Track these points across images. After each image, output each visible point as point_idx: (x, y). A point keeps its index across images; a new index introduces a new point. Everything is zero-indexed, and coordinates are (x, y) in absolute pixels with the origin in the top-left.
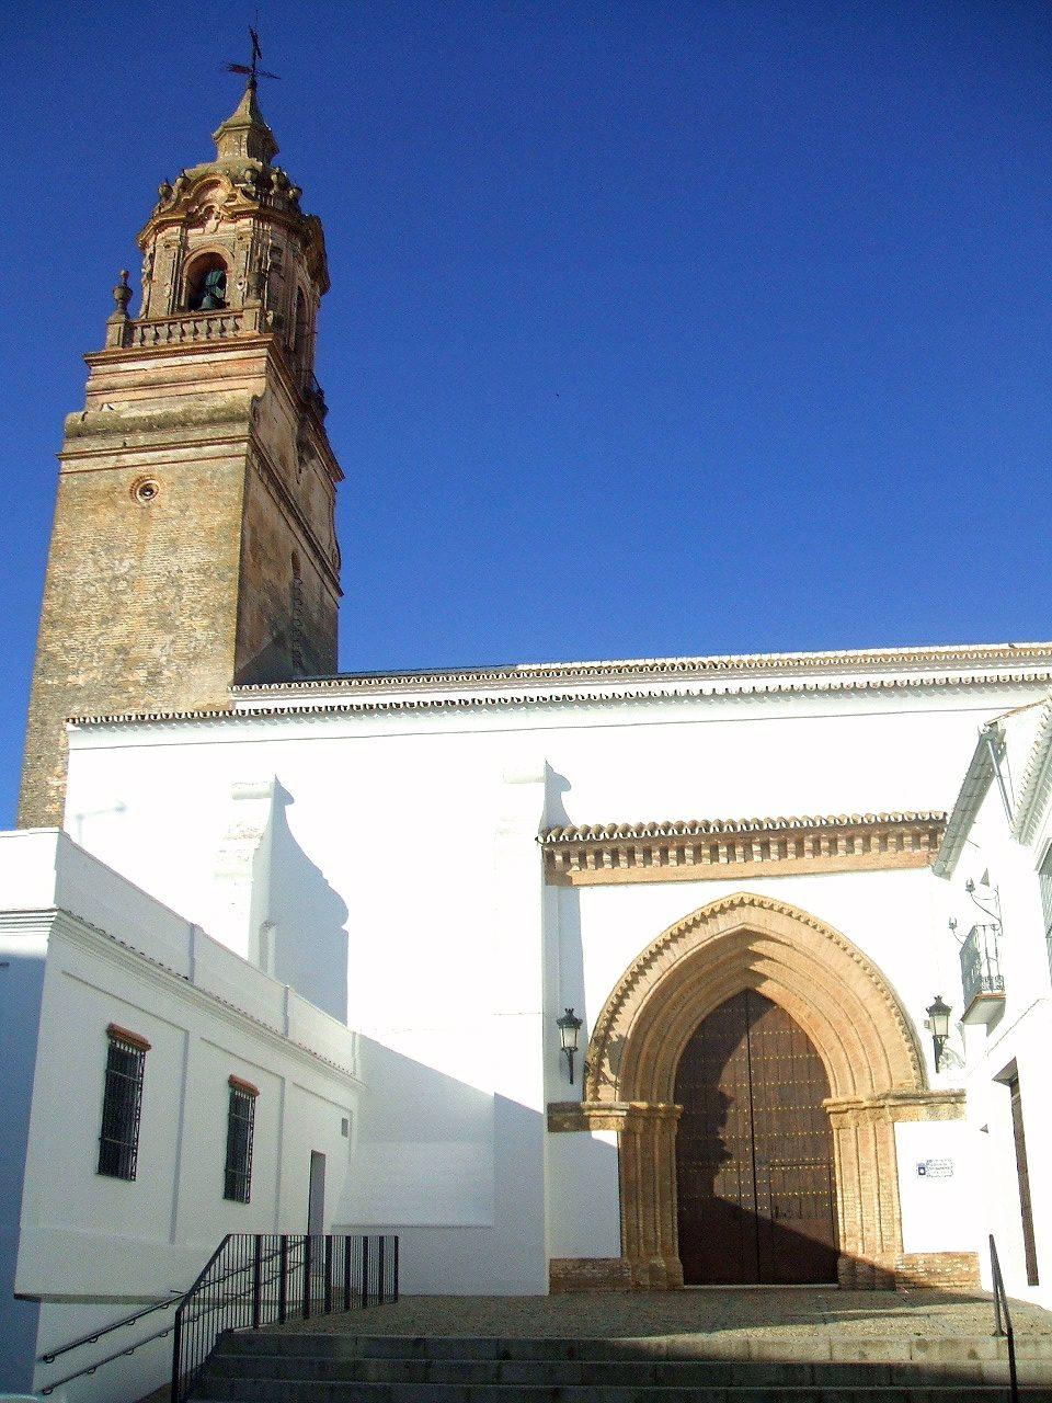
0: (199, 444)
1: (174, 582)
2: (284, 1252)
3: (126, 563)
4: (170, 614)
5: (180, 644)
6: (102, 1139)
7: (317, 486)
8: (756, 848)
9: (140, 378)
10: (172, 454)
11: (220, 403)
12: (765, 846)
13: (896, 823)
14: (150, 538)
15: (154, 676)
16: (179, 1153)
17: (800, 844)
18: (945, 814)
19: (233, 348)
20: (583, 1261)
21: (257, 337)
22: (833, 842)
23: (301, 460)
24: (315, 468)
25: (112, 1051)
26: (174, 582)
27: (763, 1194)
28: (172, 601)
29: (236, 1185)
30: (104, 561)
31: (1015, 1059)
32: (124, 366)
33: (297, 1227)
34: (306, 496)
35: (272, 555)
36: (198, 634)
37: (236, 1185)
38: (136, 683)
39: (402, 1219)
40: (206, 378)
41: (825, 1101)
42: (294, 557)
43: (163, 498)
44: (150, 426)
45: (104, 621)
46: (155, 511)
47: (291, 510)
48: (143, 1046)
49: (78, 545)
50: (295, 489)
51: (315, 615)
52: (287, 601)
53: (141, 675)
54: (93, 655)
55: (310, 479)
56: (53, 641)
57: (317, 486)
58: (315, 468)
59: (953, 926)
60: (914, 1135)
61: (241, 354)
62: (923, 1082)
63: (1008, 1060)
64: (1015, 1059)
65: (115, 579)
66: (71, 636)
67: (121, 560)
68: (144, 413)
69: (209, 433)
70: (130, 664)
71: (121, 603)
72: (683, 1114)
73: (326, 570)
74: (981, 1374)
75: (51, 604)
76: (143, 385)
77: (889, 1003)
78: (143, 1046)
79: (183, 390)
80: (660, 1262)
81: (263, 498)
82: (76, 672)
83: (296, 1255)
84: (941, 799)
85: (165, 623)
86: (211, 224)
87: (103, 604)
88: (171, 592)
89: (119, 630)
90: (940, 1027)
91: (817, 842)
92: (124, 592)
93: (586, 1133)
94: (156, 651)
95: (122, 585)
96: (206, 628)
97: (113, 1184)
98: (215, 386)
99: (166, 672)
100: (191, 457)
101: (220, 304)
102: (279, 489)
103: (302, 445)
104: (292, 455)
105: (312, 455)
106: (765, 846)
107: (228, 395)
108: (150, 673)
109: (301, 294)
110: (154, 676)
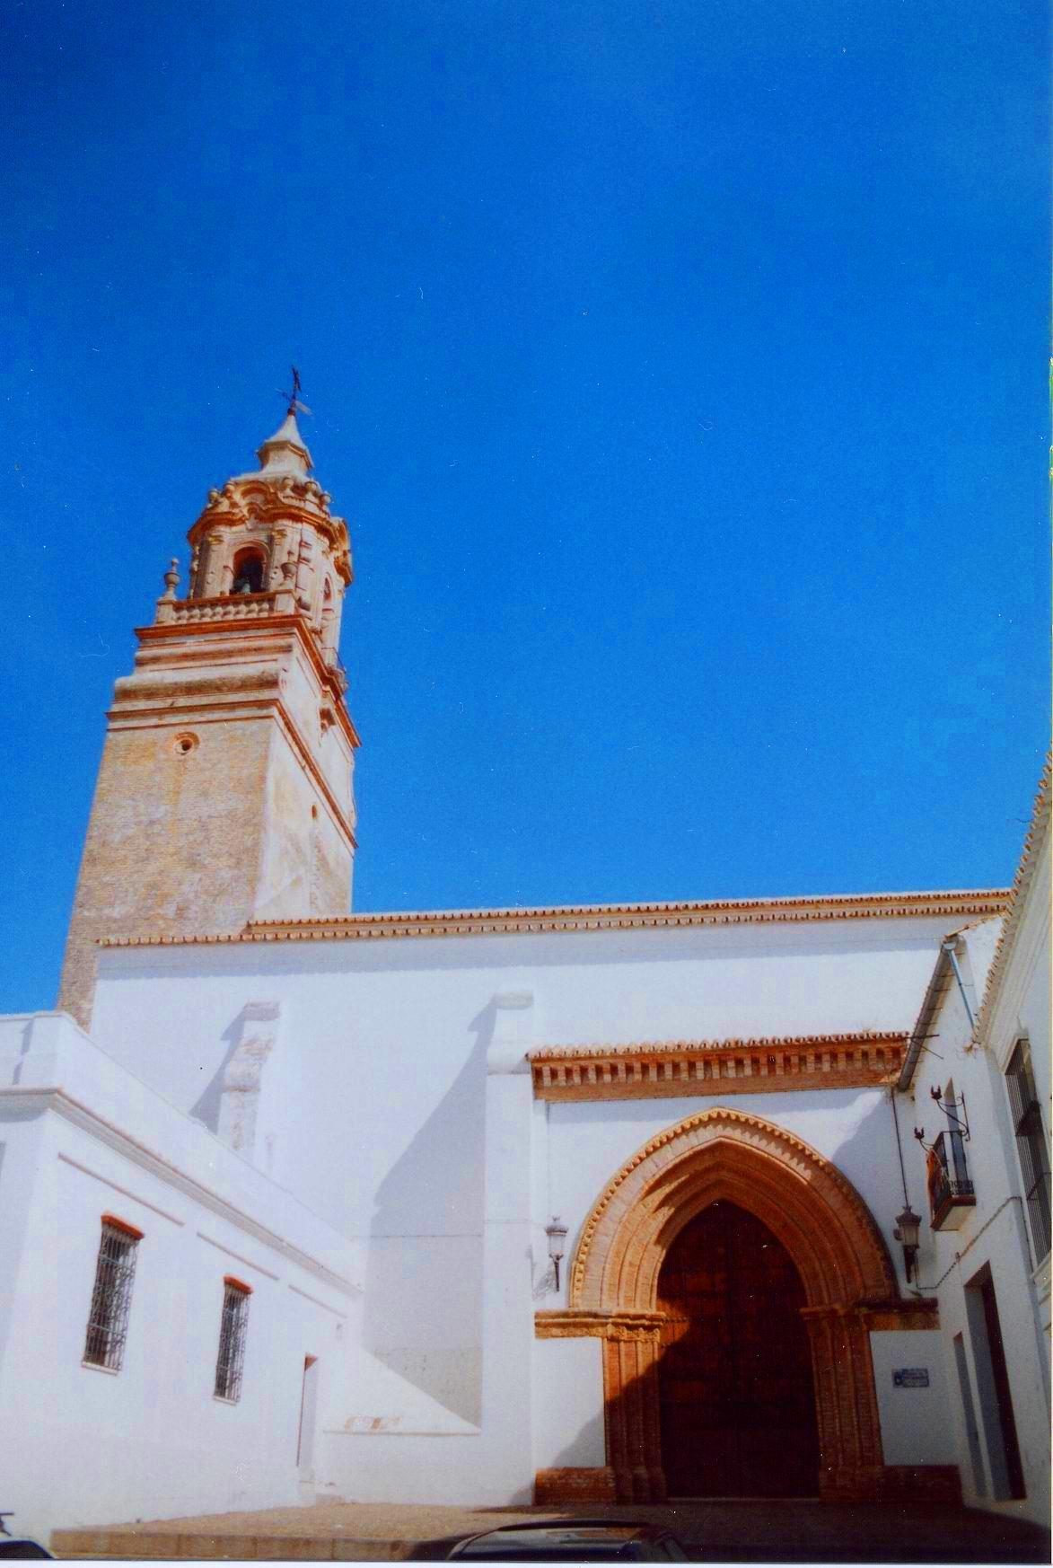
3: (162, 809)
8: (731, 1064)
15: (181, 912)
16: (220, 1247)
23: (323, 726)
26: (204, 826)
30: (142, 807)
36: (223, 873)
38: (164, 918)
48: (136, 1236)
50: (316, 753)
53: (170, 910)
56: (88, 877)
59: (919, 1136)
60: (890, 1347)
62: (895, 1287)
65: (152, 823)
74: (238, 1326)
75: (92, 845)
77: (859, 1213)
80: (642, 1471)
84: (900, 1018)
85: (193, 863)
89: (152, 868)
90: (908, 1238)
91: (787, 1060)
94: (185, 888)
95: (157, 828)
99: (194, 908)
102: (301, 749)
104: (316, 721)
105: (332, 722)
106: (739, 1063)
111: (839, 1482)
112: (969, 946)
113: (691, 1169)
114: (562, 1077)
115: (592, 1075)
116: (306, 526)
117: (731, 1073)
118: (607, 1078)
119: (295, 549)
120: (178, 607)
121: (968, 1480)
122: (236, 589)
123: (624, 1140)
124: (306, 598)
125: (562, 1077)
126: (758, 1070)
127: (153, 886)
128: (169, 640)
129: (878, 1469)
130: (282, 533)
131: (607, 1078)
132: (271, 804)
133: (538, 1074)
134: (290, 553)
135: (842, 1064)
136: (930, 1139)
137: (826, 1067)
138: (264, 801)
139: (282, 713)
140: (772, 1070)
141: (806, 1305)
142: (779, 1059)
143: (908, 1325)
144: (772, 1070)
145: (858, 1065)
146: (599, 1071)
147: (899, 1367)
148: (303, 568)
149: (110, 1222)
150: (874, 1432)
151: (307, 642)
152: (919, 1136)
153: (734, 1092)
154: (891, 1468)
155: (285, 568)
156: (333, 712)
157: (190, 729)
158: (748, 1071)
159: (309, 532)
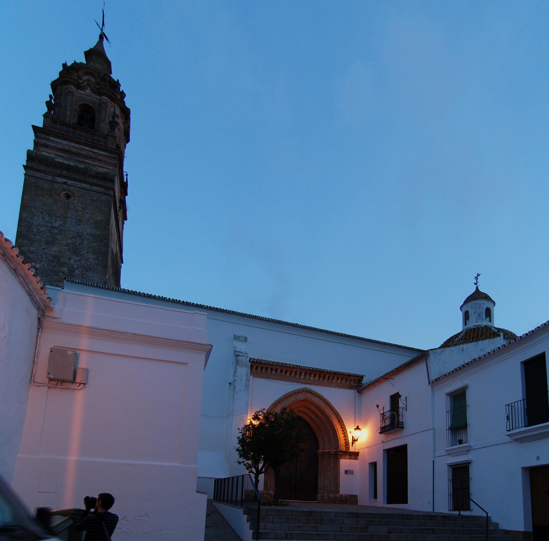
0: (92, 184)
3: (58, 223)
4: (78, 249)
5: (83, 262)
8: (312, 375)
10: (79, 184)
12: (315, 375)
14: (69, 215)
17: (324, 377)
21: (114, 149)
28: (80, 244)
31: (33, 126)
32: (52, 138)
36: (91, 260)
44: (68, 168)
45: (47, 243)
49: (34, 208)
53: (66, 269)
54: (42, 256)
59: (378, 406)
63: (364, 374)
64: (33, 126)
66: (32, 245)
67: (56, 221)
69: (95, 181)
79: (80, 159)
87: (47, 236)
88: (79, 241)
89: (55, 249)
91: (329, 377)
93: (209, 498)
94: (72, 262)
95: (56, 231)
96: (94, 259)
98: (95, 163)
99: (77, 271)
100: (88, 188)
106: (315, 375)
108: (69, 270)
111: (325, 498)
115: (269, 370)
117: (312, 378)
118: (274, 372)
123: (268, 394)
125: (261, 368)
127: (55, 257)
128: (526, 416)
129: (338, 495)
131: (274, 372)
133: (252, 367)
140: (324, 379)
142: (327, 376)
143: (350, 459)
145: (348, 383)
146: (272, 369)
147: (347, 469)
153: (311, 384)
154: (341, 495)
157: (72, 188)
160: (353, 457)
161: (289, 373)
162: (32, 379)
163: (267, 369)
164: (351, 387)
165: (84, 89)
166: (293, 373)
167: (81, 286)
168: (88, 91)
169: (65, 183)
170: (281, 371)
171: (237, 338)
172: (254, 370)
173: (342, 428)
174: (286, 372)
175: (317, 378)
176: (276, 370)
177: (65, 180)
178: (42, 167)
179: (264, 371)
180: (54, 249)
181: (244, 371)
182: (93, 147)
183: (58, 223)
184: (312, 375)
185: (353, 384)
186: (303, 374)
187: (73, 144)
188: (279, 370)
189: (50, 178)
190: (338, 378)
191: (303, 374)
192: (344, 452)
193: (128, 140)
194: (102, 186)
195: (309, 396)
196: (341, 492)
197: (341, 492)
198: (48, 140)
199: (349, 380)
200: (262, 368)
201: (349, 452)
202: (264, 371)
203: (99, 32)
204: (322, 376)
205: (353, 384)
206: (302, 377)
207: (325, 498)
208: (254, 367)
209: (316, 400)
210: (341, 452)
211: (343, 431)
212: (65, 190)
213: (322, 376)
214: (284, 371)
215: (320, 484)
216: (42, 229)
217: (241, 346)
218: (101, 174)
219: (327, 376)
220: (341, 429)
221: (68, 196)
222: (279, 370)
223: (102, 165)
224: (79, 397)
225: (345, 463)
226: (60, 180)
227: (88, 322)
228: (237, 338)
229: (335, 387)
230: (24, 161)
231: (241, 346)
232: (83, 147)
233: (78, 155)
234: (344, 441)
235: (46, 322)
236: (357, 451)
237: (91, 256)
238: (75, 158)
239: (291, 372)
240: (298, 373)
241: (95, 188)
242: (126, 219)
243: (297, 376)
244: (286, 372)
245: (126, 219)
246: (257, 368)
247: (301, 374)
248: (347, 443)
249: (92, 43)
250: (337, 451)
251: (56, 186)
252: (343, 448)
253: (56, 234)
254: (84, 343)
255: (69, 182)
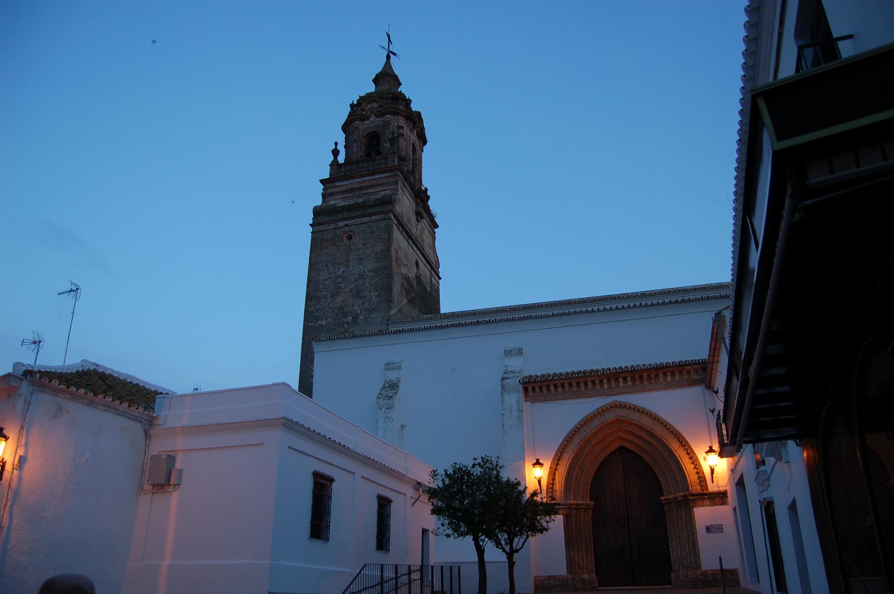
1: (362, 276)
2: (409, 574)
3: (341, 270)
5: (366, 305)
6: (311, 522)
7: (426, 231)
8: (620, 380)
9: (344, 188)
11: (378, 196)
12: (625, 379)
13: (686, 365)
17: (641, 377)
18: (336, 144)
19: (384, 172)
20: (549, 577)
22: (657, 376)
23: (418, 220)
24: (425, 222)
25: (315, 483)
27: (180, 443)
29: (382, 542)
30: (331, 270)
32: (337, 184)
33: (416, 561)
34: (421, 236)
35: (405, 262)
37: (382, 542)
38: (348, 323)
39: (460, 560)
40: (372, 186)
41: (662, 498)
42: (417, 263)
43: (355, 240)
44: (348, 208)
45: (333, 296)
46: (353, 246)
47: (414, 243)
48: (332, 480)
51: (428, 289)
52: (414, 282)
53: (350, 319)
55: (422, 229)
57: (426, 231)
58: (425, 222)
61: (387, 174)
68: (346, 204)
69: (374, 210)
70: (345, 315)
71: (340, 288)
72: (514, 488)
73: (432, 268)
76: (346, 192)
78: (332, 480)
79: (363, 192)
80: (585, 576)
81: (431, 257)
82: (321, 319)
83: (416, 576)
84: (703, 354)
85: (358, 294)
86: (372, 118)
91: (649, 376)
92: (340, 283)
94: (356, 308)
95: (340, 280)
97: (317, 544)
101: (379, 153)
103: (418, 215)
104: (413, 218)
105: (422, 218)
106: (625, 379)
107: (383, 193)
109: (413, 145)
110: (355, 319)
111: (681, 578)
112: (50, 574)
113: (577, 440)
114: (538, 388)
115: (552, 388)
116: (400, 117)
117: (621, 384)
118: (560, 390)
119: (396, 130)
120: (377, 116)
121: (741, 577)
122: (368, 155)
124: (403, 154)
125: (538, 388)
126: (635, 382)
127: (341, 308)
130: (389, 122)
131: (560, 390)
132: (394, 263)
133: (526, 390)
134: (393, 133)
135: (677, 377)
136: (716, 413)
137: (669, 379)
138: (391, 261)
139: (395, 216)
140: (642, 382)
141: (663, 495)
144: (642, 382)
145: (685, 377)
146: (556, 386)
147: (709, 524)
148: (401, 140)
149: (316, 475)
150: (697, 555)
151: (407, 179)
152: (712, 411)
153: (623, 393)
154: (705, 572)
155: (390, 140)
156: (422, 212)
157: (352, 228)
158: (629, 383)
159: (402, 122)
160: (717, 500)
161: (582, 385)
162: (141, 488)
163: (548, 387)
164: (693, 383)
165: (368, 119)
166: (590, 384)
167: (329, 342)
168: (372, 118)
169: (347, 225)
170: (570, 385)
171: (508, 353)
172: (531, 394)
173: (688, 454)
174: (578, 384)
175: (629, 383)
176: (563, 385)
177: (345, 222)
178: (326, 219)
179: (545, 392)
180: (338, 300)
181: (515, 398)
182: (374, 174)
183: (341, 270)
184: (620, 380)
185: (696, 377)
186: (605, 381)
187: (356, 180)
188: (566, 385)
189: (333, 226)
190: (665, 374)
191: (605, 381)
192: (697, 495)
193: (424, 142)
194: (381, 213)
195: (622, 413)
196: (704, 568)
197: (704, 568)
198: (333, 187)
199: (684, 372)
200: (541, 388)
201: (706, 494)
202: (545, 392)
203: (386, 53)
204: (637, 377)
205: (696, 377)
206: (606, 386)
207: (681, 578)
208: (530, 389)
209: (634, 417)
210: (692, 495)
211: (691, 458)
212: (346, 232)
213: (637, 377)
214: (574, 384)
215: (673, 558)
216: (327, 283)
217: (515, 363)
218: (379, 199)
219: (645, 376)
220: (687, 456)
221: (350, 238)
222: (566, 385)
223: (384, 188)
224: (174, 498)
225: (703, 514)
226: (341, 224)
227: (184, 422)
228: (508, 353)
229: (665, 389)
230: (309, 218)
231: (515, 363)
232: (364, 179)
233: (360, 189)
234: (696, 476)
235: (152, 432)
236: (722, 489)
237: (373, 294)
238: (358, 193)
239: (586, 383)
240: (597, 382)
241: (374, 217)
242: (437, 226)
243: (598, 387)
244: (578, 384)
245: (437, 226)
246: (534, 389)
247: (601, 382)
248: (702, 479)
249: (379, 68)
250: (686, 496)
251: (338, 232)
252: (697, 488)
253: (340, 283)
254: (180, 443)
255: (349, 222)
